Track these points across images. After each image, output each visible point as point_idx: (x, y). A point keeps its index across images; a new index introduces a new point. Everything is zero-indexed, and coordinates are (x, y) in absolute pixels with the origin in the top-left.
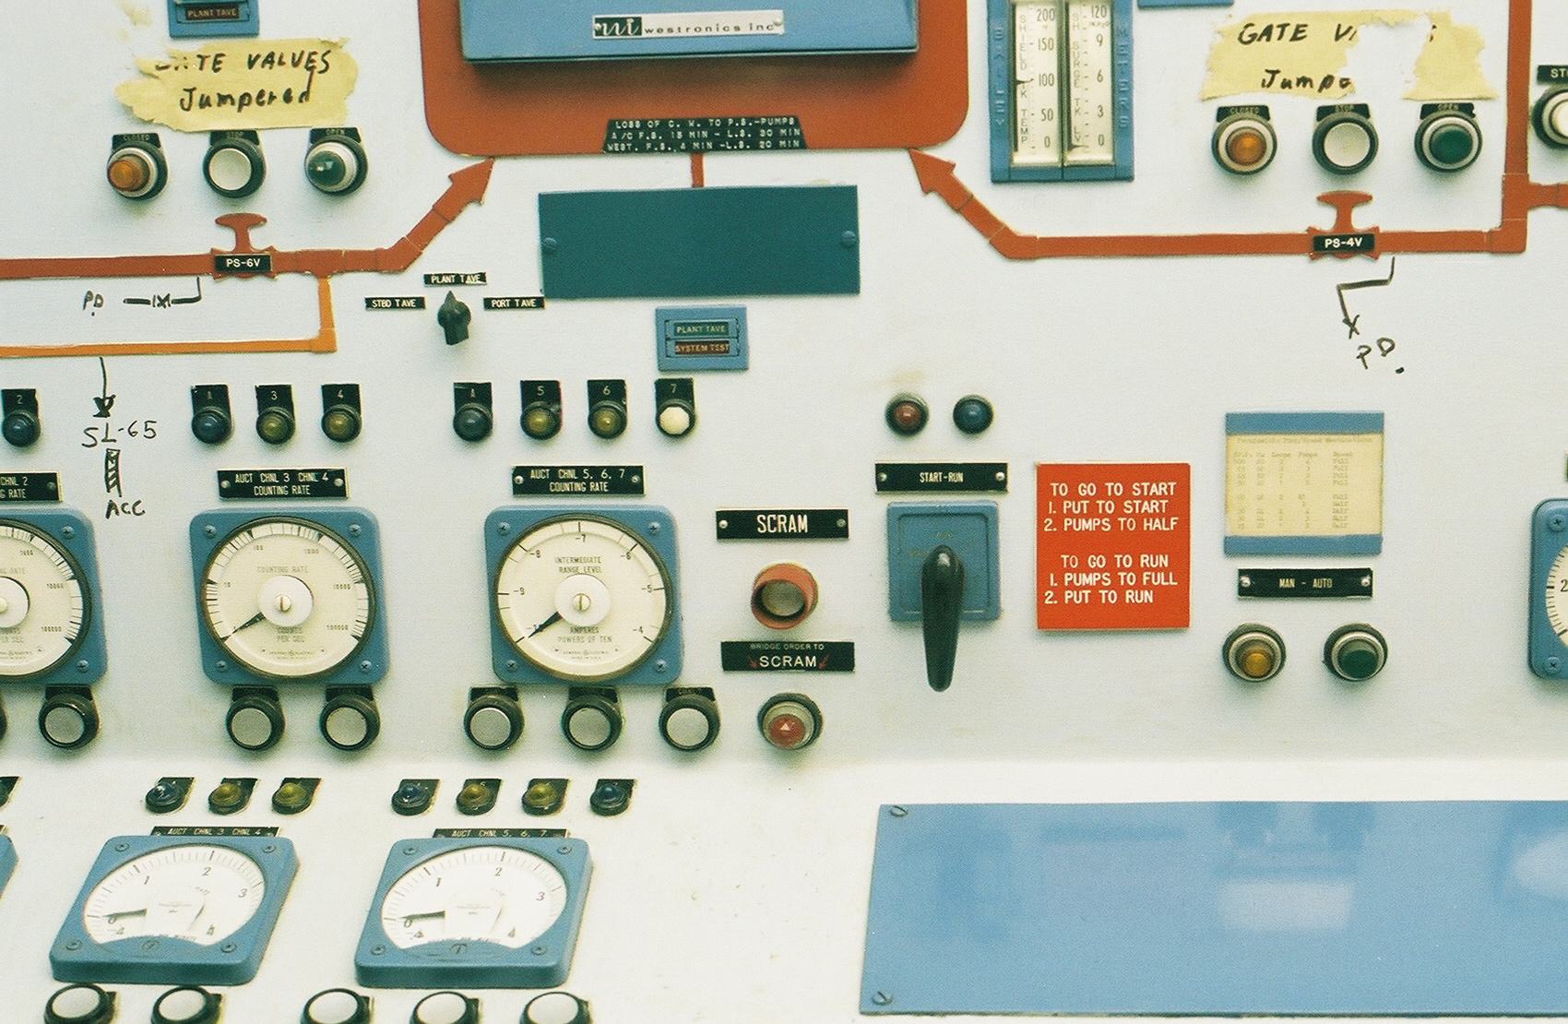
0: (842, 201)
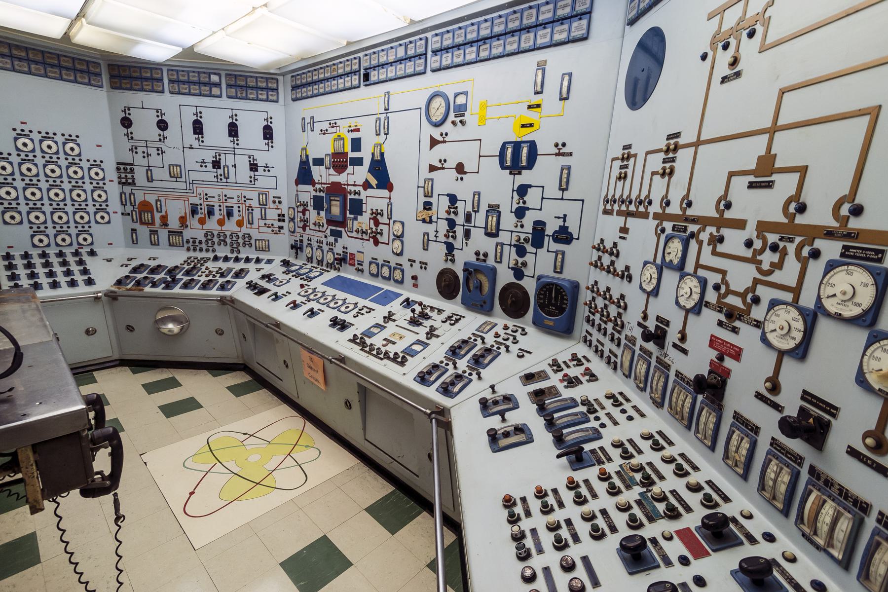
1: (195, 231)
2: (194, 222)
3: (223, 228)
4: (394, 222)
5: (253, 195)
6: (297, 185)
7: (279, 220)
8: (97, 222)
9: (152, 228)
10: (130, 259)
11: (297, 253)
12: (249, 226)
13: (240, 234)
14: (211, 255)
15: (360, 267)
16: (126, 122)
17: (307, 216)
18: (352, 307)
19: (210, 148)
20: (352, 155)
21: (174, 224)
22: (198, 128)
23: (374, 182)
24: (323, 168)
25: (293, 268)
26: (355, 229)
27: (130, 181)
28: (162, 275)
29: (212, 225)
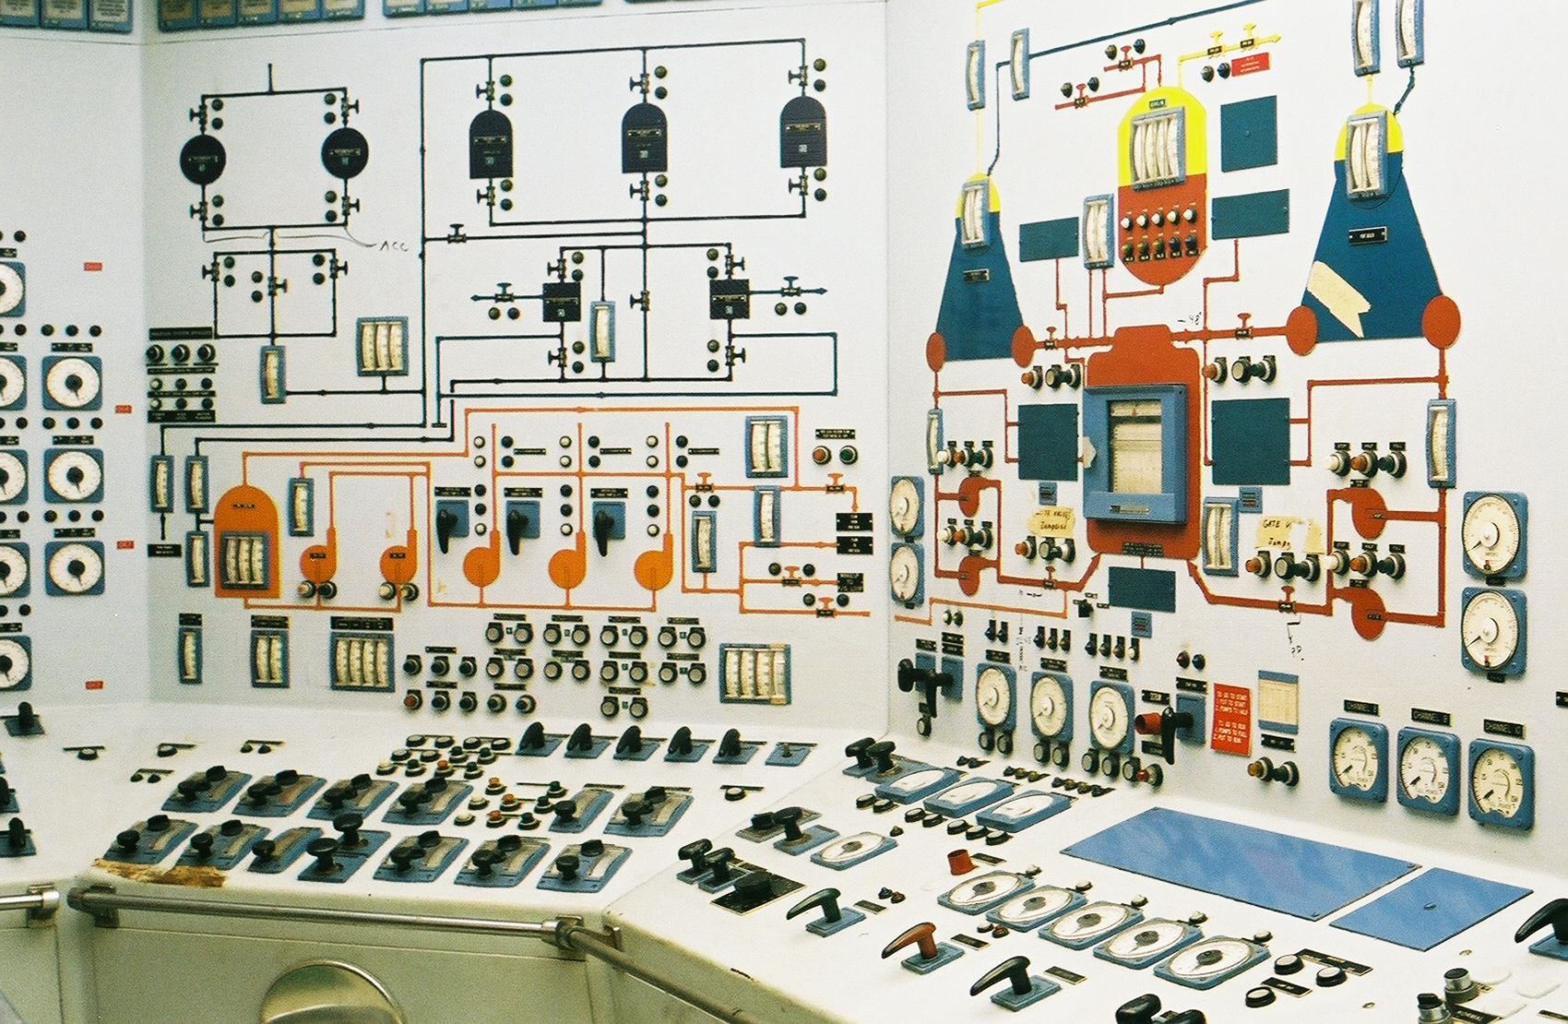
0: (1169, 578)
1: (447, 618)
2: (443, 572)
3: (579, 596)
4: (1471, 500)
5: (719, 428)
6: (936, 367)
7: (844, 546)
8: (53, 589)
9: (265, 607)
10: (167, 751)
11: (929, 710)
12: (695, 580)
13: (653, 624)
14: (513, 727)
15: (1279, 758)
16: (203, 160)
17: (986, 511)
18: (1234, 955)
19: (533, 231)
20: (1224, 185)
21: (359, 588)
22: (491, 148)
23: (1348, 304)
24: (1073, 267)
25: (908, 783)
26: (1247, 553)
27: (194, 404)
28: (299, 819)
29: (525, 581)
